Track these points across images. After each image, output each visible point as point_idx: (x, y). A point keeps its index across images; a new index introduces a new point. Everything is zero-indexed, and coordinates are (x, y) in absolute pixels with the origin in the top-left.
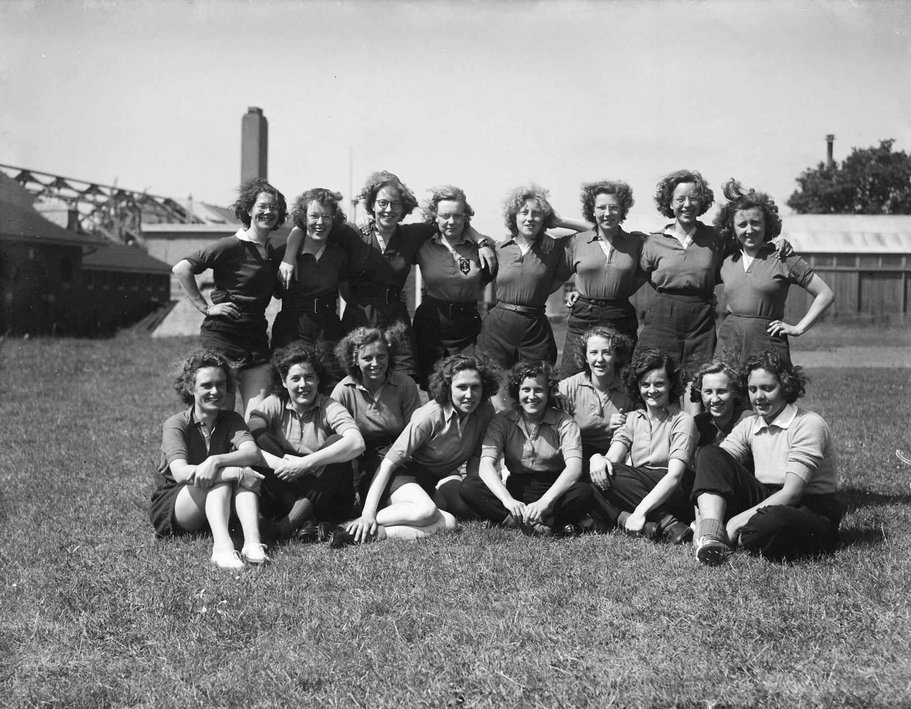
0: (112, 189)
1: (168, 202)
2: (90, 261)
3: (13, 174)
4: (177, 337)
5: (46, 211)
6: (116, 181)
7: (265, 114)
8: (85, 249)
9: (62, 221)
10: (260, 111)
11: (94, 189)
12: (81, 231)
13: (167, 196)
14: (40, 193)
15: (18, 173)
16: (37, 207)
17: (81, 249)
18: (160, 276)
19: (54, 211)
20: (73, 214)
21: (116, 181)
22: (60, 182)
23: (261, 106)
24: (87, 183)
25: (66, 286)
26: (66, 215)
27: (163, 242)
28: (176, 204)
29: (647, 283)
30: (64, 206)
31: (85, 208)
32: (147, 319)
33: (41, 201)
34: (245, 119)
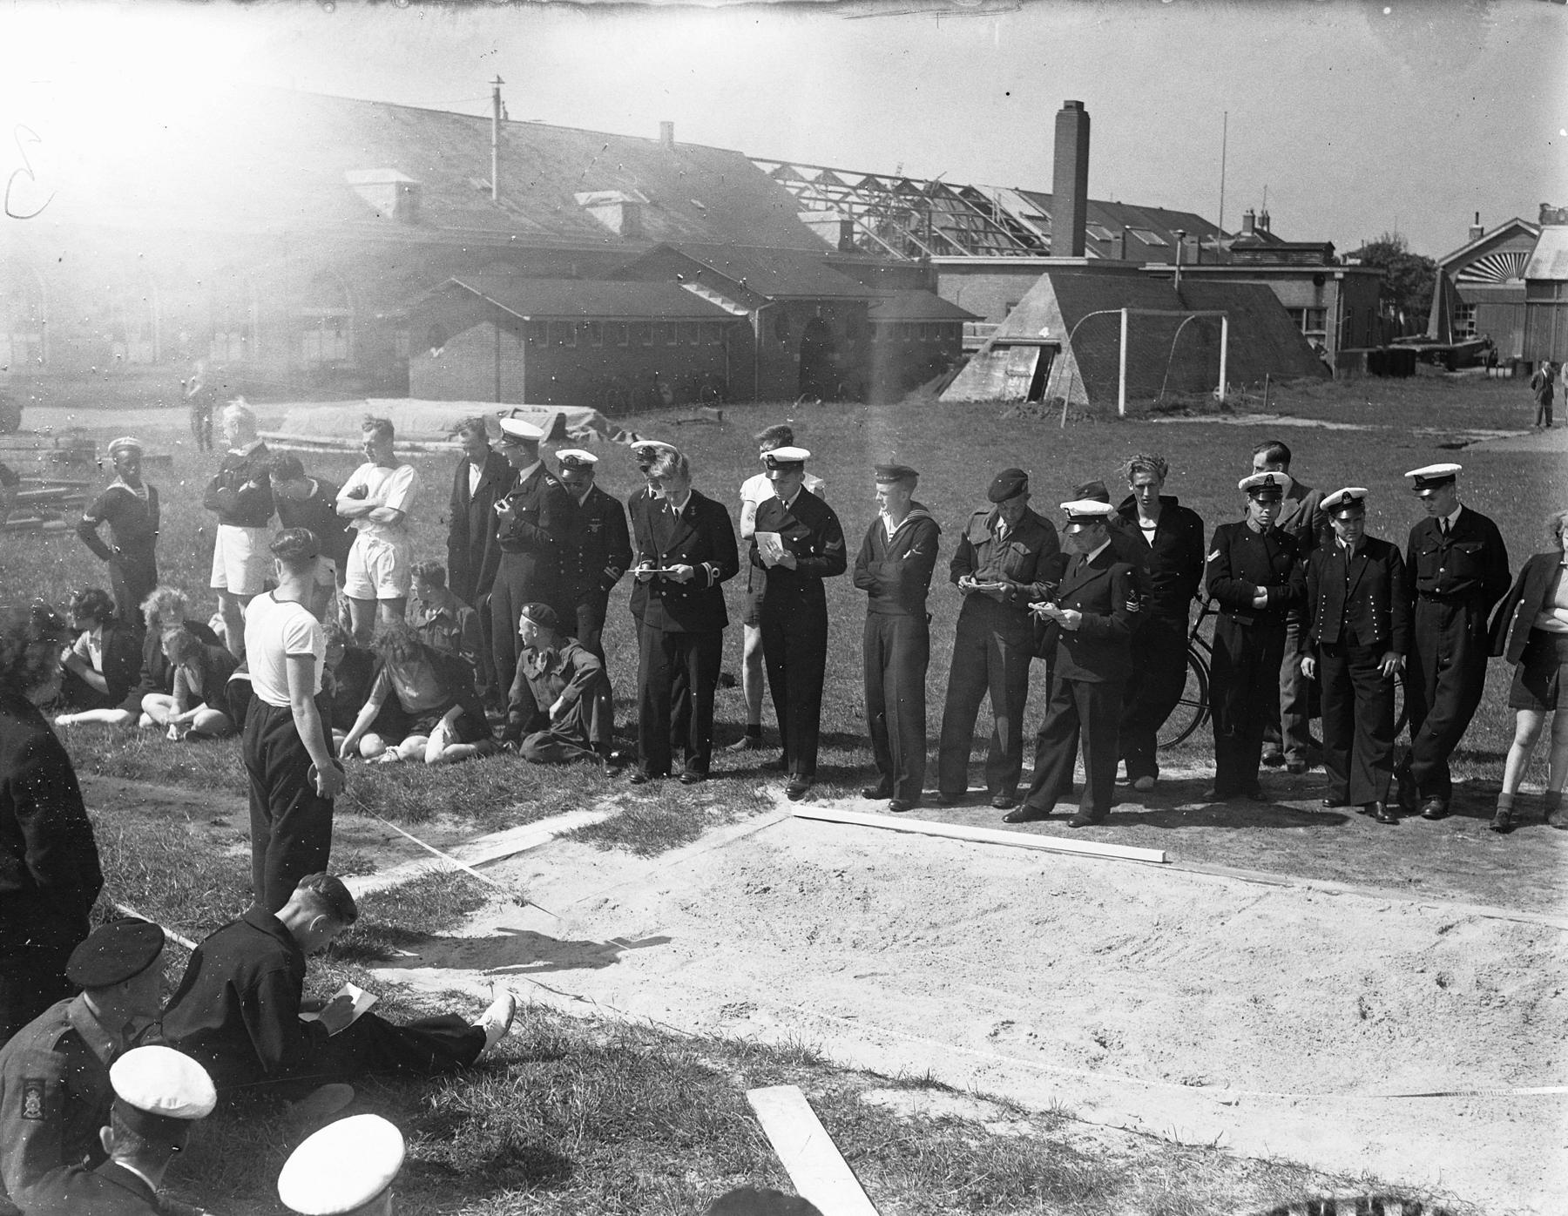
10: (1080, 105)
20: (846, 227)
26: (838, 227)
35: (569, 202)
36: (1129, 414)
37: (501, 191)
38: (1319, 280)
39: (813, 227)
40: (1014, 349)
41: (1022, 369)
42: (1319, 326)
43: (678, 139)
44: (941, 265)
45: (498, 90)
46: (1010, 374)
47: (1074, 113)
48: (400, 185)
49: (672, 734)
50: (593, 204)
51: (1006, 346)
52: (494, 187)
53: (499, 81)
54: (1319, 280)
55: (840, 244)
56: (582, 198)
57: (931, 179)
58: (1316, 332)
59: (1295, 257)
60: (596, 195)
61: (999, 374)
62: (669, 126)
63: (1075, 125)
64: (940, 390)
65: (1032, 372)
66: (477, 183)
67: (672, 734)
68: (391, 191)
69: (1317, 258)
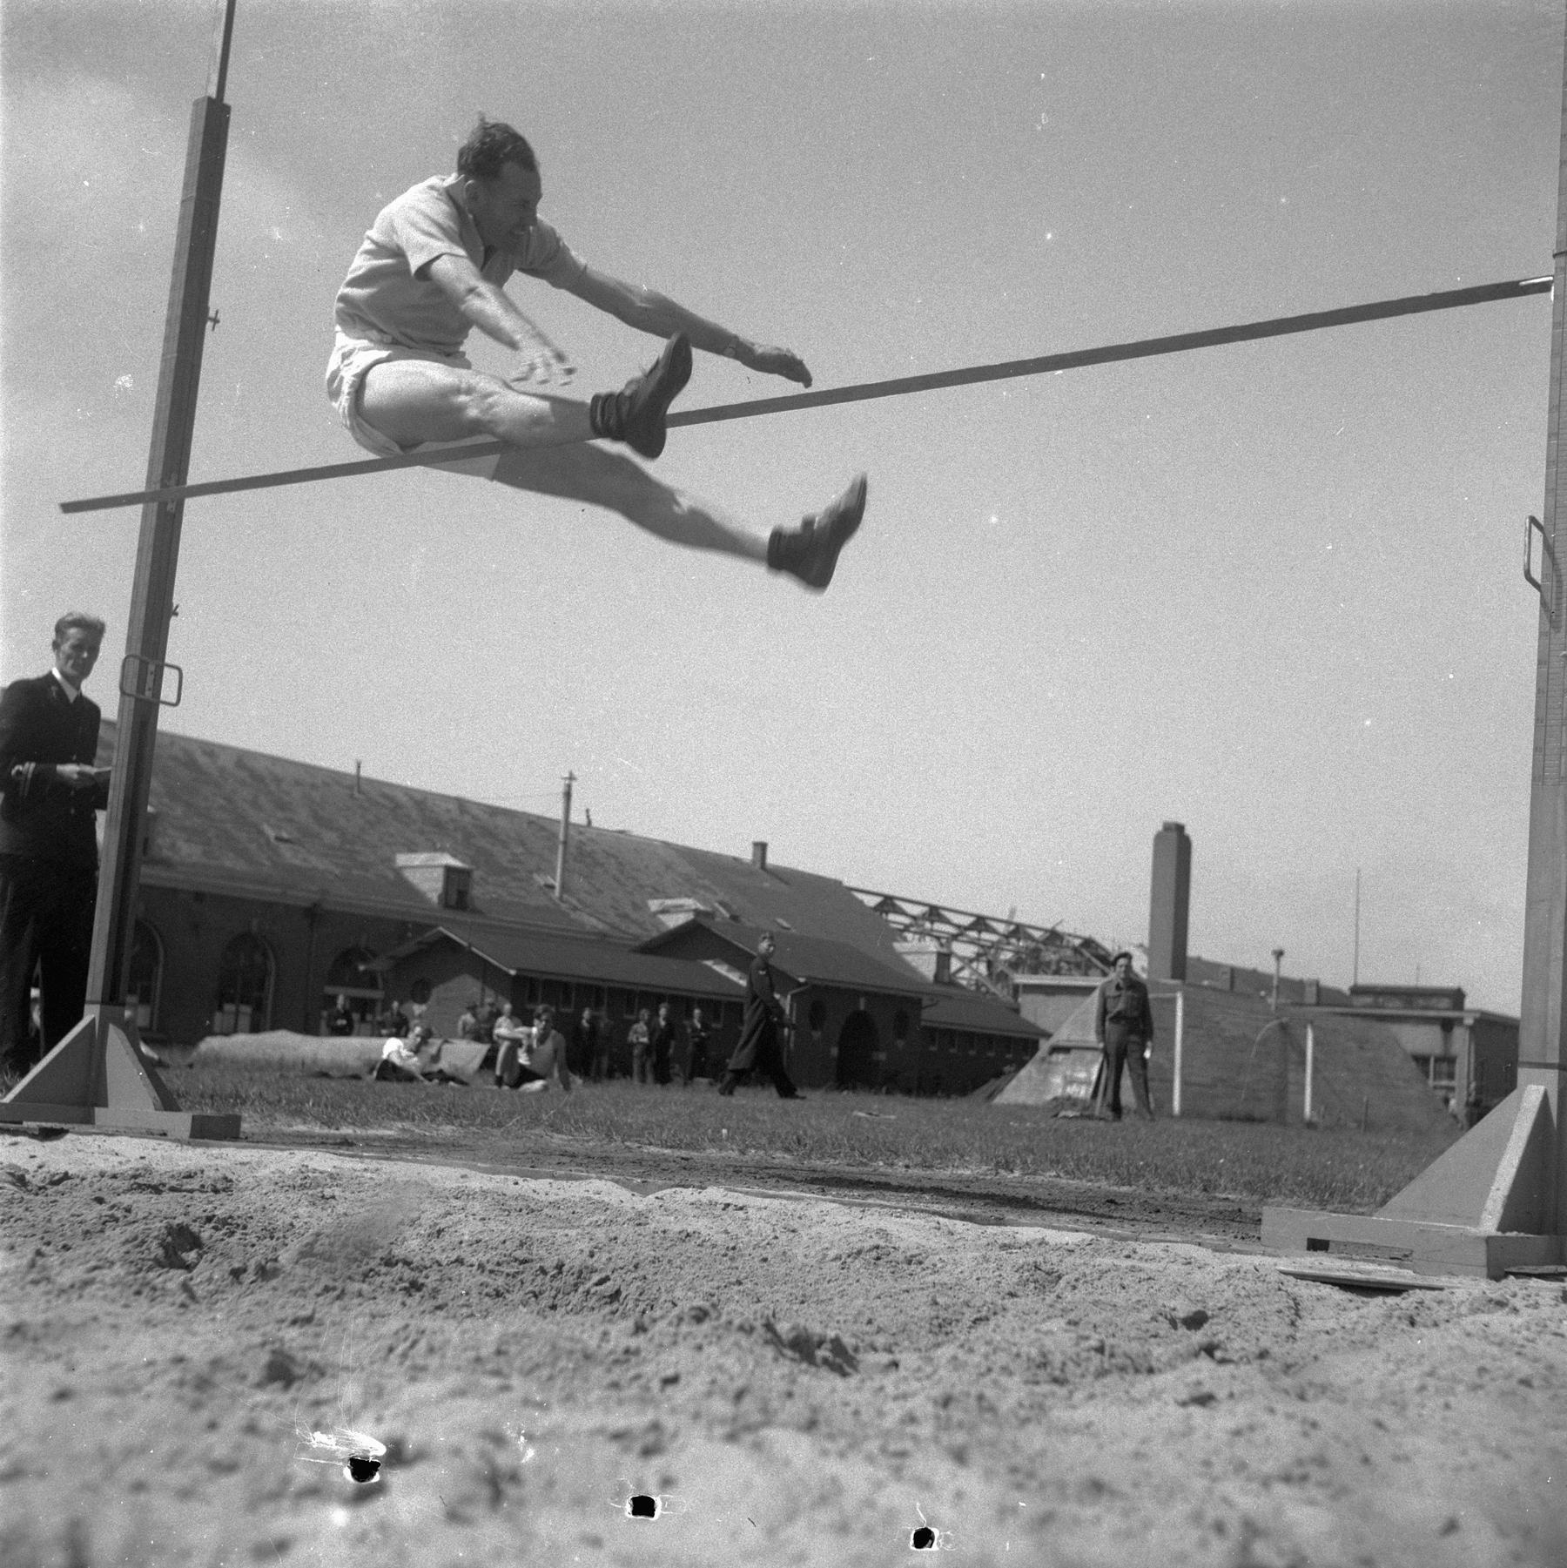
0: (1008, 923)
1: (1088, 943)
2: (930, 1016)
3: (872, 901)
4: (313, 914)
5: (909, 953)
6: (1013, 912)
7: (1188, 831)
8: (925, 1002)
9: (927, 968)
10: (1180, 828)
11: (981, 923)
12: (952, 983)
13: (1087, 934)
14: (907, 928)
15: (878, 900)
16: (898, 946)
17: (920, 1000)
18: (1026, 1041)
19: (920, 956)
20: (944, 959)
21: (1013, 912)
22: (934, 913)
23: (1182, 821)
24: (971, 915)
25: (900, 1043)
26: (934, 958)
27: (1040, 998)
28: (1098, 946)
29: (1557, 1061)
30: (932, 945)
31: (963, 949)
32: (984, 1088)
33: (905, 939)
34: (1159, 838)
35: (639, 907)
36: (1185, 1113)
37: (565, 888)
38: (1447, 1025)
39: (909, 958)
40: (1074, 1053)
41: (1082, 1075)
42: (1451, 1076)
43: (772, 859)
44: (1025, 986)
45: (569, 787)
46: (1069, 1081)
47: (1174, 835)
48: (449, 870)
49: (36, 1016)
50: (665, 911)
51: (1066, 1050)
52: (557, 885)
53: (571, 778)
54: (1447, 1025)
55: (936, 976)
56: (654, 905)
57: (1049, 926)
58: (1444, 1083)
59: (1421, 1002)
60: (669, 902)
61: (1057, 1080)
62: (761, 848)
63: (1175, 846)
64: (991, 1096)
65: (1094, 1077)
66: (540, 880)
67: (36, 1016)
68: (439, 874)
69: (1445, 1002)
